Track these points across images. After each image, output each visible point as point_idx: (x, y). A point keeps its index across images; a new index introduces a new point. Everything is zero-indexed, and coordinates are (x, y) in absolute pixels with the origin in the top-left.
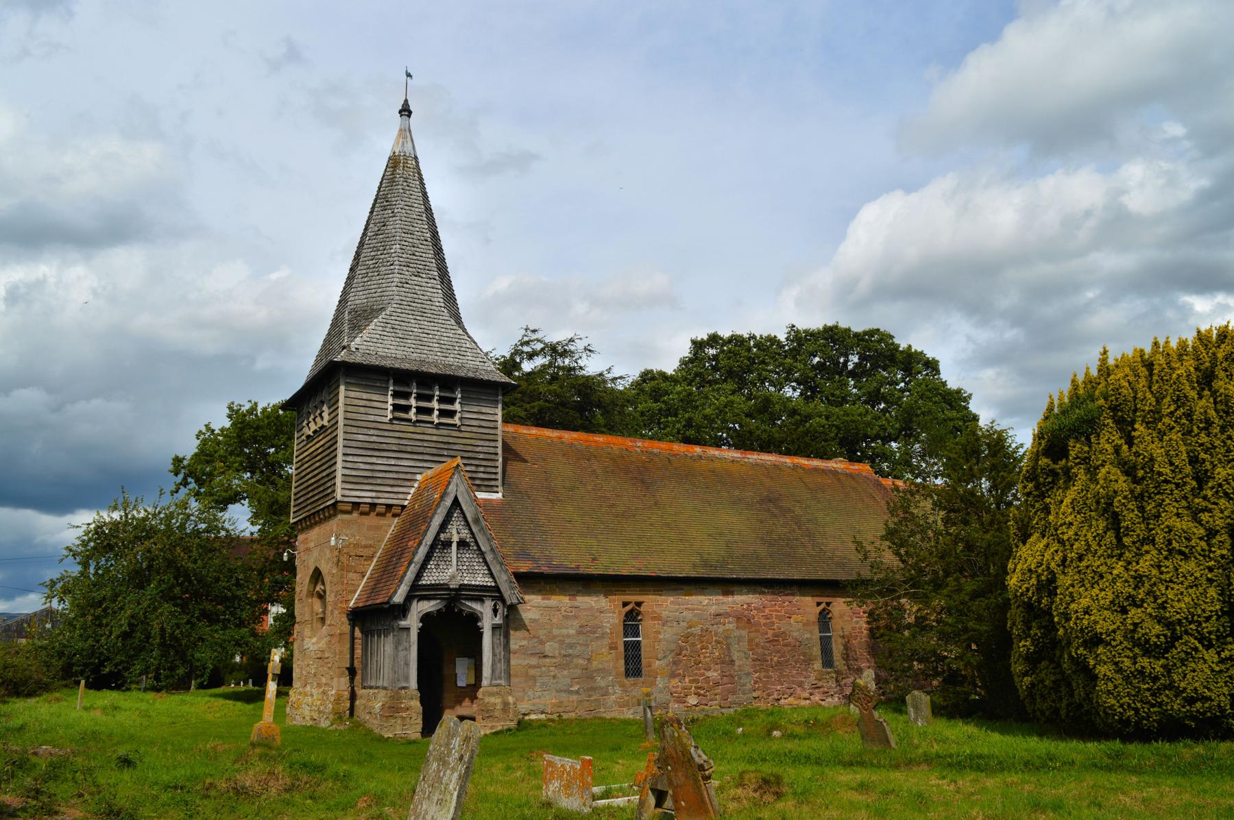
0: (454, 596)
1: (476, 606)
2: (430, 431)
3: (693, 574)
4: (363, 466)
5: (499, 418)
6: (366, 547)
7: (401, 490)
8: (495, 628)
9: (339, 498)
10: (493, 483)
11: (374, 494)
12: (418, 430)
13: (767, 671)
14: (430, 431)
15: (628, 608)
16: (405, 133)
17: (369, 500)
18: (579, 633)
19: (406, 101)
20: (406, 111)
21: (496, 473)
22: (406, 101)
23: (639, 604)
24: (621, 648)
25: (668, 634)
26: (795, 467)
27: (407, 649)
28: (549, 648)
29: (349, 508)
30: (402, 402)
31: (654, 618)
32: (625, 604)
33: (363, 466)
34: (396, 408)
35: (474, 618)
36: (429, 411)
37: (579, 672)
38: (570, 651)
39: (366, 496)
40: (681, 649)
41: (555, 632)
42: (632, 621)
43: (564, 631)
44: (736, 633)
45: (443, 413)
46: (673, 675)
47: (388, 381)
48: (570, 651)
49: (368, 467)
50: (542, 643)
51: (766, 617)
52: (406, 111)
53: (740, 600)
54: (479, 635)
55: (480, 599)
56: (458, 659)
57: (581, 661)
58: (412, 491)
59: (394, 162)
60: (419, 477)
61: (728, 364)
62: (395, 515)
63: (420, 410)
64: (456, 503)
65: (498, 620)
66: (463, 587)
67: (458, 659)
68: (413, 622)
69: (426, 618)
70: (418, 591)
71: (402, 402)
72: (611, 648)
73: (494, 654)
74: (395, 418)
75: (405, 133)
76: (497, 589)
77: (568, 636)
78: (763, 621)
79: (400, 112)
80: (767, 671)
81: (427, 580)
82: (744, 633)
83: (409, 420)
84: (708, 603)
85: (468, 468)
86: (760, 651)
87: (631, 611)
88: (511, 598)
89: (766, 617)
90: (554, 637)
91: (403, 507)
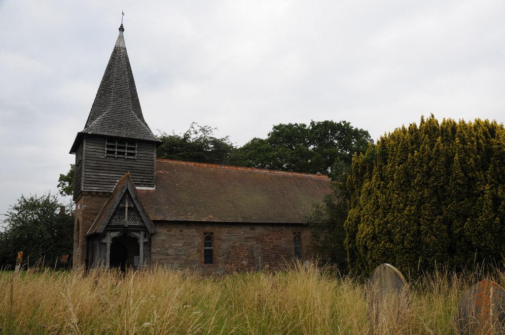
0: (126, 231)
1: (137, 234)
2: (122, 162)
3: (300, 222)
4: (93, 177)
5: (155, 156)
6: (94, 210)
7: (110, 186)
8: (145, 243)
9: (82, 189)
10: (151, 183)
11: (98, 188)
12: (127, 162)
13: (269, 261)
14: (122, 162)
15: (207, 235)
16: (121, 38)
17: (96, 191)
18: (184, 245)
19: (122, 24)
20: (122, 29)
21: (85, 172)
22: (122, 24)
23: (212, 233)
24: (203, 252)
25: (224, 246)
26: (294, 176)
27: (106, 252)
28: (170, 251)
29: (101, 194)
30: (111, 150)
31: (218, 240)
32: (205, 234)
33: (93, 177)
34: (108, 152)
35: (136, 240)
36: (123, 154)
37: (183, 261)
38: (179, 253)
39: (95, 189)
40: (230, 252)
41: (173, 245)
42: (209, 239)
43: (177, 245)
44: (256, 245)
45: (119, 153)
46: (226, 263)
47: (105, 141)
48: (179, 253)
49: (96, 177)
50: (167, 249)
51: (270, 239)
52: (122, 29)
53: (259, 231)
54: (139, 247)
55: (138, 231)
56: (135, 257)
57: (184, 257)
58: (115, 186)
59: (116, 50)
60: (118, 181)
61: (286, 135)
62: (107, 197)
63: (119, 153)
64: (127, 190)
65: (146, 240)
66: (130, 226)
67: (135, 257)
68: (108, 241)
69: (114, 239)
70: (109, 228)
71: (111, 150)
72: (198, 252)
73: (144, 255)
74: (107, 156)
75: (121, 38)
76: (145, 227)
77: (179, 247)
78: (268, 241)
79: (119, 29)
80: (269, 261)
81: (114, 223)
82: (259, 245)
83: (114, 157)
84: (242, 232)
85: (132, 176)
86: (266, 253)
87: (208, 236)
88: (151, 231)
89: (270, 239)
90: (172, 247)
91: (111, 193)
